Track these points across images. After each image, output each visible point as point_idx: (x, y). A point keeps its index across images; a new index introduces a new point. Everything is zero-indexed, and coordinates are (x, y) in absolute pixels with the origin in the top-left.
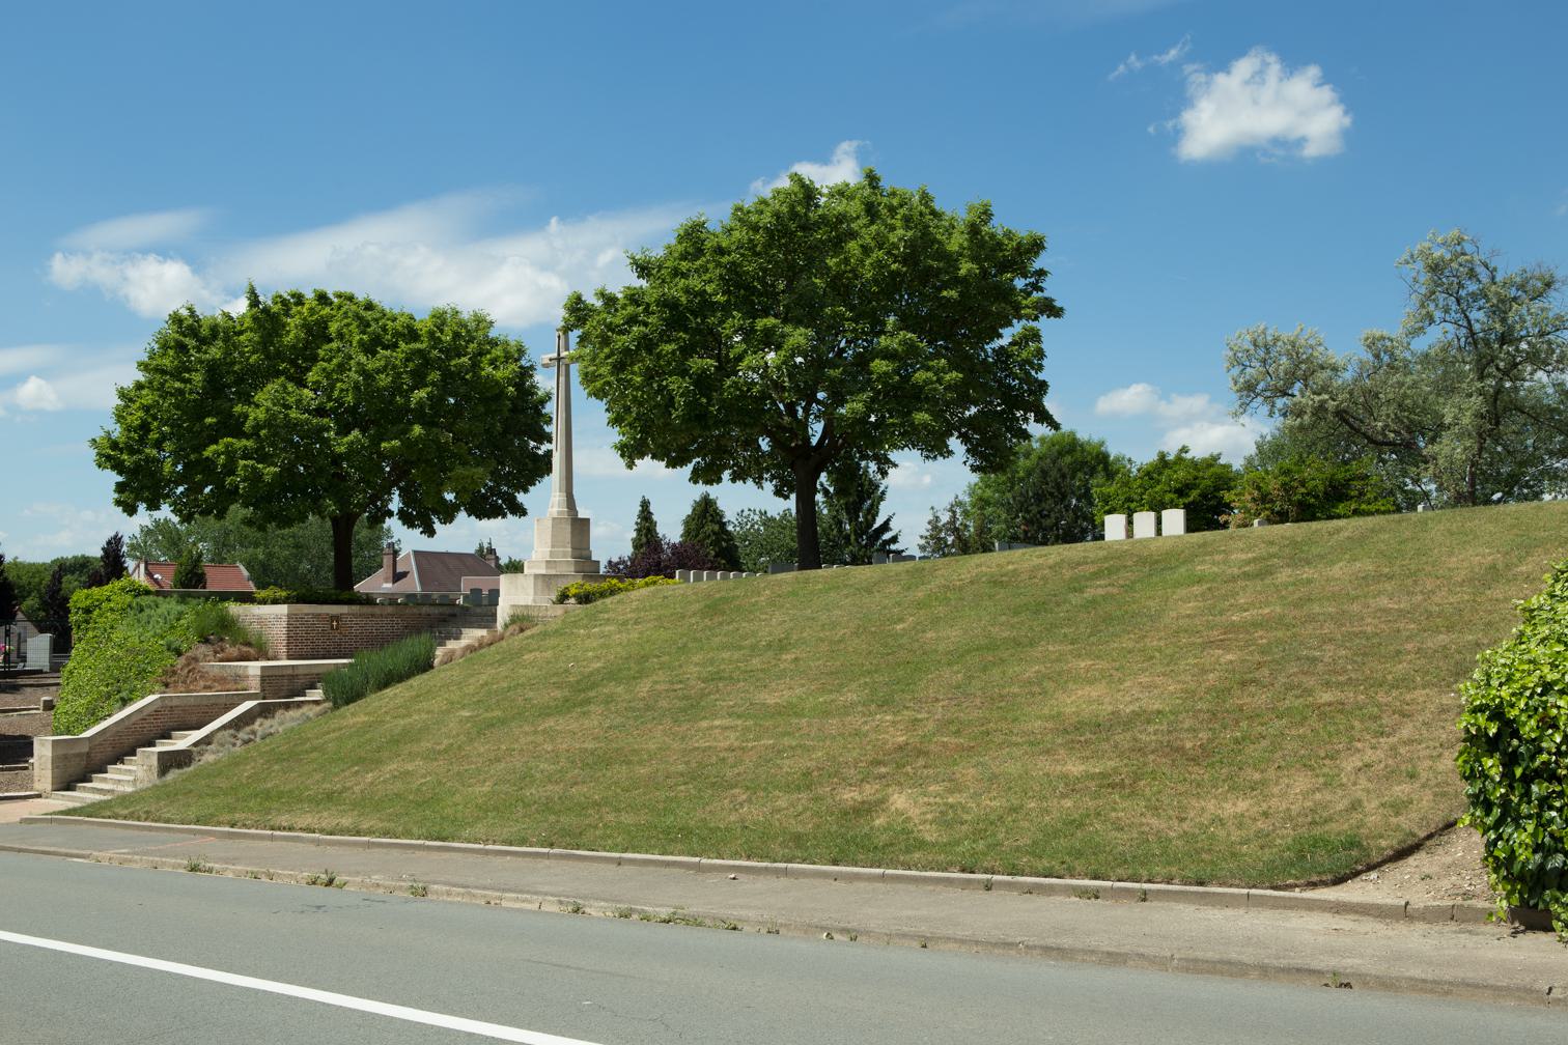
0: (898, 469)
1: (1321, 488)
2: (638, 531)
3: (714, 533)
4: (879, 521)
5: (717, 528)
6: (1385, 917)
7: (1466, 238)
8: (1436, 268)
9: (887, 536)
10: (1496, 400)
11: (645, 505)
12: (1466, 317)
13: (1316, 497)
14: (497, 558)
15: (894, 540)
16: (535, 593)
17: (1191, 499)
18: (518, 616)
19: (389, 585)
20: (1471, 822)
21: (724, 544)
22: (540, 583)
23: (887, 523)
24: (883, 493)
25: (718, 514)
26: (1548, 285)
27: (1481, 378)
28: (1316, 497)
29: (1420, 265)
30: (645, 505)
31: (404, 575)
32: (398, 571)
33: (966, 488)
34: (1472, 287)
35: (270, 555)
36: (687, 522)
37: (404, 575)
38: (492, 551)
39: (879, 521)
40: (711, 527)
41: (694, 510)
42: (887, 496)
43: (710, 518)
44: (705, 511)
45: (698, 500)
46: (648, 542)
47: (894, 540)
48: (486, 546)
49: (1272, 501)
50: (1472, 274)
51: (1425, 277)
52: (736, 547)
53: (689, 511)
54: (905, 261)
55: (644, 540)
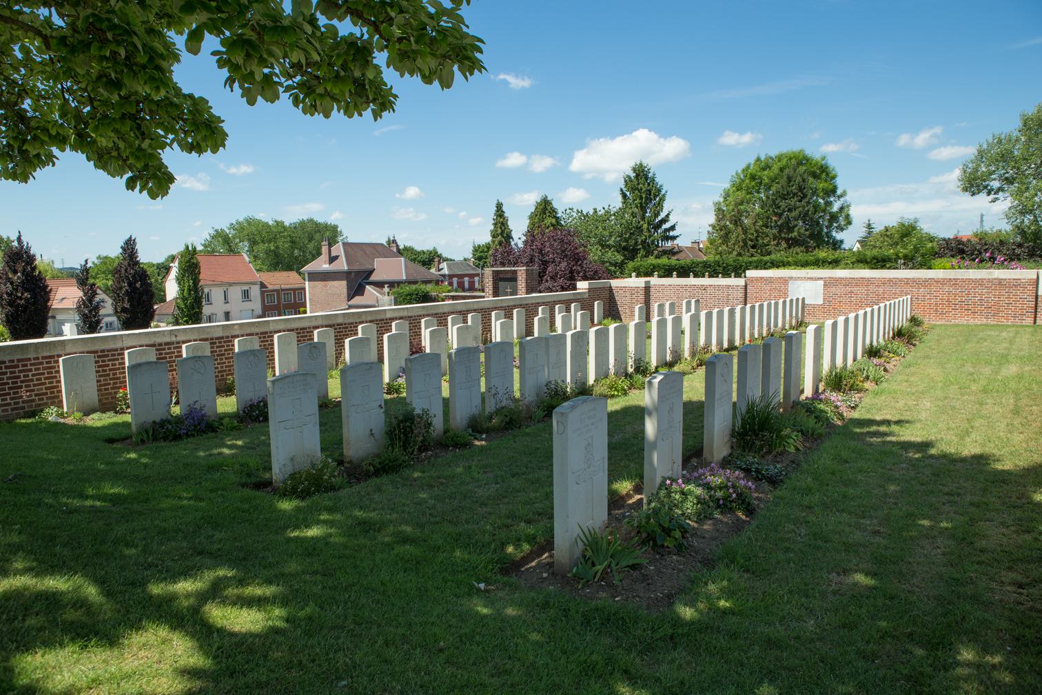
0: (847, 190)
2: (495, 224)
3: (553, 225)
4: (662, 215)
5: (554, 221)
6: (820, 354)
9: (665, 226)
11: (499, 206)
14: (397, 246)
15: (673, 228)
19: (327, 266)
20: (53, 404)
23: (668, 216)
24: (664, 195)
25: (554, 211)
30: (499, 206)
31: (336, 257)
33: (722, 192)
35: (277, 247)
37: (336, 257)
38: (394, 241)
39: (662, 215)
40: (549, 221)
41: (536, 208)
43: (548, 214)
44: (544, 211)
45: (539, 201)
46: (503, 232)
47: (673, 228)
48: (392, 239)
55: (499, 231)
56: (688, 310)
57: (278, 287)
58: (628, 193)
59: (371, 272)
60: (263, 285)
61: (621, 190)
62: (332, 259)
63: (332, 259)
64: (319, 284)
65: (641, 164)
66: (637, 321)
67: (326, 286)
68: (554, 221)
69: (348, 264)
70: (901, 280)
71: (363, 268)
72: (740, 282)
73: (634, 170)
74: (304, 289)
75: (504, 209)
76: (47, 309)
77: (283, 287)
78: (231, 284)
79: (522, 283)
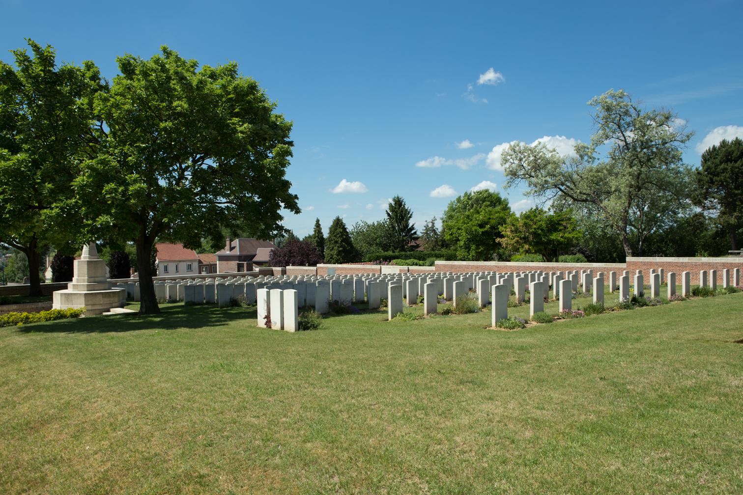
1: (544, 225)
3: (341, 232)
7: (625, 94)
8: (608, 109)
9: (413, 232)
10: (638, 178)
11: (318, 221)
12: (623, 135)
13: (542, 230)
16: (61, 304)
17: (486, 229)
18: (507, 205)
21: (344, 237)
22: (63, 297)
26: (667, 118)
27: (631, 167)
28: (542, 230)
29: (599, 108)
30: (318, 221)
31: (234, 248)
32: (232, 246)
34: (628, 119)
36: (330, 229)
37: (234, 248)
42: (413, 216)
44: (337, 224)
47: (415, 233)
49: (520, 232)
50: (627, 113)
51: (603, 114)
52: (350, 238)
53: (332, 224)
54: (159, 84)
55: (317, 235)
56: (533, 280)
57: (208, 263)
58: (391, 213)
59: (254, 256)
60: (200, 262)
61: (387, 211)
62: (232, 249)
63: (232, 249)
64: (224, 263)
65: (398, 197)
66: (494, 287)
67: (227, 264)
68: (341, 230)
69: (240, 251)
70: (353, 268)
71: (249, 254)
72: (315, 268)
73: (394, 200)
74: (216, 265)
75: (320, 223)
76: (727, 125)
77: (211, 263)
78: (180, 261)
79: (245, 268)
